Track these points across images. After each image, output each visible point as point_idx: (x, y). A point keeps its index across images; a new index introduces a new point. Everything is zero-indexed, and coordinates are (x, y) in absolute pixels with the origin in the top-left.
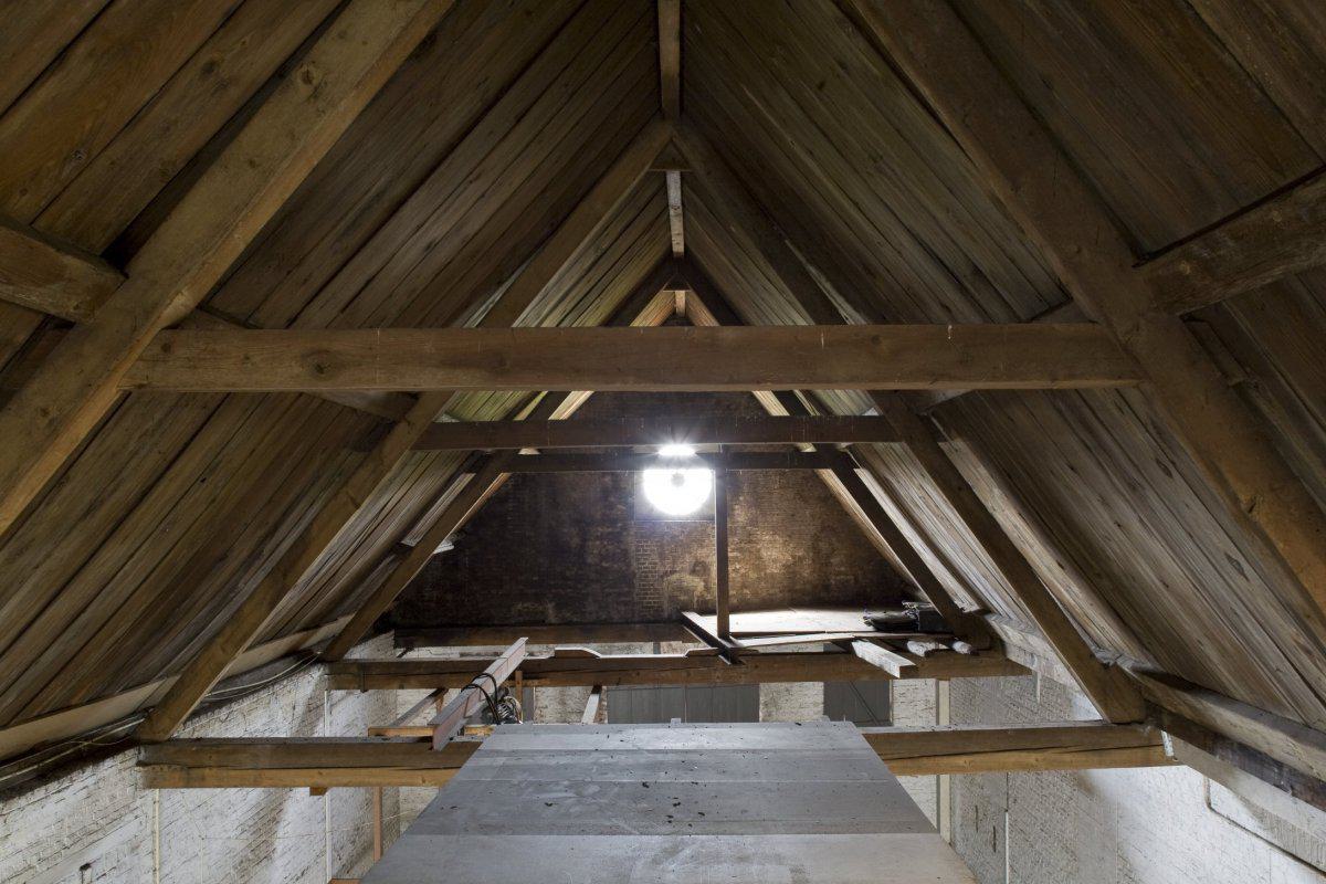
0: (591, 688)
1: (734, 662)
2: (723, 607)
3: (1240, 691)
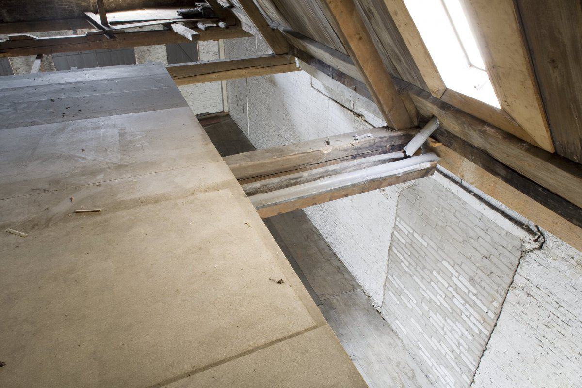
0: (35, 56)
1: (111, 37)
2: (103, 11)
3: (317, 38)
